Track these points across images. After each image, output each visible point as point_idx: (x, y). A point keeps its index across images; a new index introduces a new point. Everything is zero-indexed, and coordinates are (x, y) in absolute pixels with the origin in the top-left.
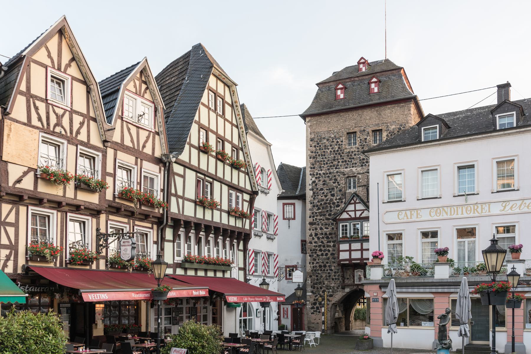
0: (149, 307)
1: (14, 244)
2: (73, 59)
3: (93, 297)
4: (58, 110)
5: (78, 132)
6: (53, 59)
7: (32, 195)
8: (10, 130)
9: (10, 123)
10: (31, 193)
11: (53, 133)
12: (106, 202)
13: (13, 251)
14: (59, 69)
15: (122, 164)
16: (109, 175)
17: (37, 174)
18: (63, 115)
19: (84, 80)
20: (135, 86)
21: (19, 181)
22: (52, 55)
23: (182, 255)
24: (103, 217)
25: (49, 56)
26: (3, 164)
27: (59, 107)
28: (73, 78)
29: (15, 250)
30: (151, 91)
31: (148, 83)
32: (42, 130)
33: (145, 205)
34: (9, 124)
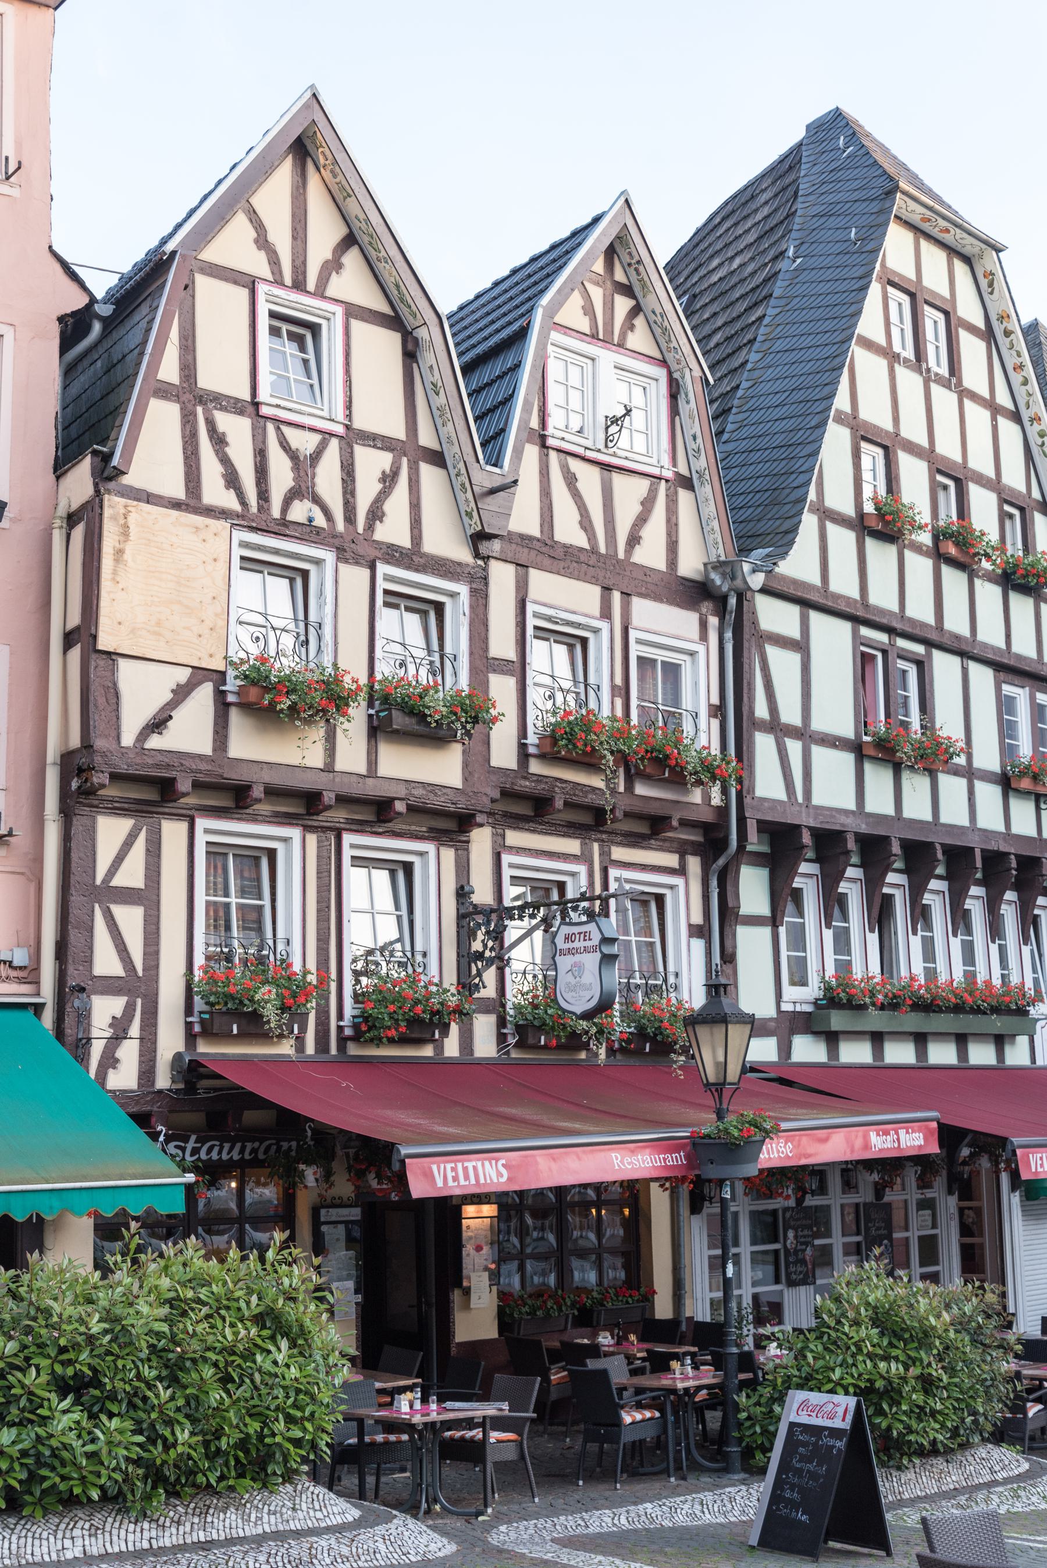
2: (350, 241)
3: (450, 1174)
5: (376, 514)
6: (275, 252)
7: (208, 774)
10: (203, 766)
11: (282, 528)
12: (494, 778)
13: (139, 1001)
14: (299, 285)
15: (549, 619)
16: (502, 666)
17: (525, 745)
18: (316, 456)
20: (588, 309)
21: (158, 724)
23: (814, 979)
24: (481, 839)
25: (262, 242)
28: (353, 311)
29: (145, 997)
31: (637, 289)
32: (240, 519)
34: (123, 511)
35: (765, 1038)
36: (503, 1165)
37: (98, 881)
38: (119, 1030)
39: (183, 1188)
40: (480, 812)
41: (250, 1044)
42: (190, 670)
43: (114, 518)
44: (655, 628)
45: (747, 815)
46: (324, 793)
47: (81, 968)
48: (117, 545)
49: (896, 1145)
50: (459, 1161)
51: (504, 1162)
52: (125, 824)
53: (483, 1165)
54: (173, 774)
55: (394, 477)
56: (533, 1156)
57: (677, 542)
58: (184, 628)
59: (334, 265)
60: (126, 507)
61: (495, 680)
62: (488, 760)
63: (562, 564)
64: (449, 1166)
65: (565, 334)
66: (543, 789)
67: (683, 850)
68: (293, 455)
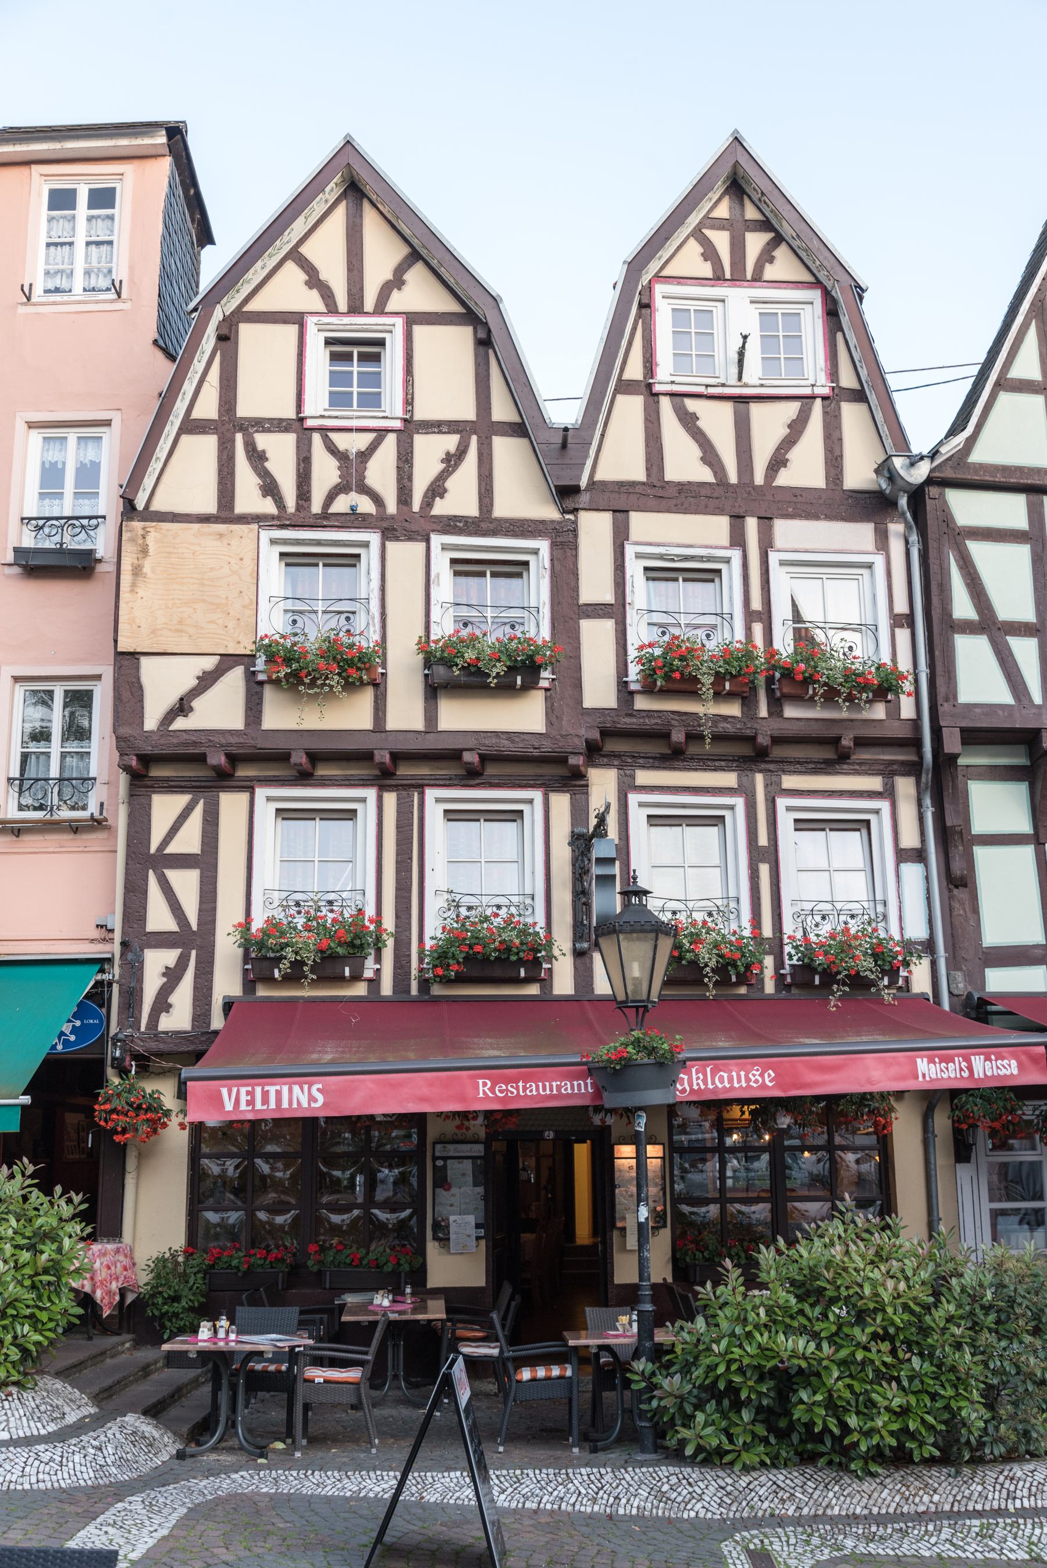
0: (943, 1159)
1: (195, 927)
2: (415, 256)
3: (244, 1098)
4: (341, 441)
6: (329, 288)
7: (240, 745)
8: (144, 551)
9: (144, 529)
10: (233, 740)
11: (325, 520)
12: (588, 719)
13: (194, 953)
14: (356, 307)
15: (661, 557)
17: (626, 682)
19: (462, 310)
20: (710, 253)
21: (182, 707)
22: (323, 276)
25: (314, 280)
26: (126, 663)
27: (349, 430)
28: (413, 319)
29: (200, 949)
30: (795, 244)
31: (774, 222)
32: (281, 521)
33: (798, 699)
34: (141, 532)
35: (1028, 967)
36: (318, 1090)
37: (153, 850)
38: (173, 976)
39: (19, 1108)
40: (572, 753)
41: (323, 988)
42: (218, 657)
43: (132, 540)
44: (855, 548)
45: (942, 724)
46: (375, 752)
47: (135, 926)
48: (136, 562)
49: (966, 1074)
50: (258, 1085)
51: (320, 1086)
52: (181, 800)
53: (290, 1091)
54: (202, 750)
55: (460, 455)
56: (363, 1081)
57: (841, 456)
58: (209, 622)
59: (397, 282)
60: (144, 529)
61: (587, 627)
62: (580, 701)
63: (674, 502)
64: (243, 1090)
65: (679, 284)
66: (656, 724)
67: (889, 771)
68: (341, 456)
